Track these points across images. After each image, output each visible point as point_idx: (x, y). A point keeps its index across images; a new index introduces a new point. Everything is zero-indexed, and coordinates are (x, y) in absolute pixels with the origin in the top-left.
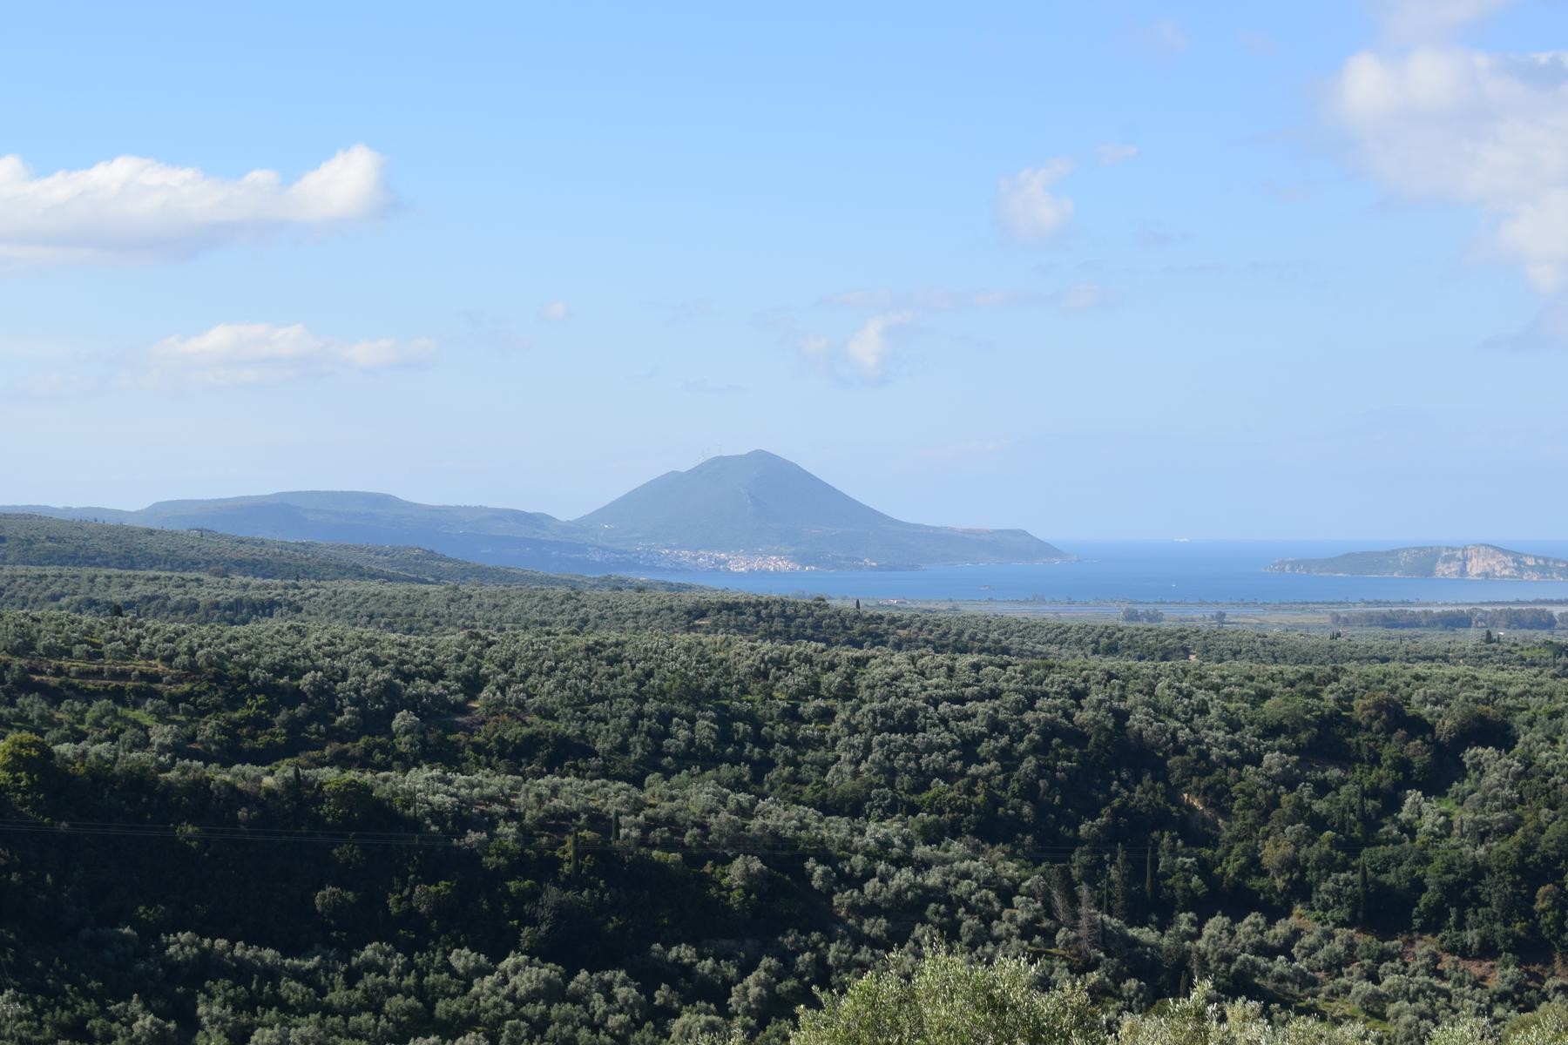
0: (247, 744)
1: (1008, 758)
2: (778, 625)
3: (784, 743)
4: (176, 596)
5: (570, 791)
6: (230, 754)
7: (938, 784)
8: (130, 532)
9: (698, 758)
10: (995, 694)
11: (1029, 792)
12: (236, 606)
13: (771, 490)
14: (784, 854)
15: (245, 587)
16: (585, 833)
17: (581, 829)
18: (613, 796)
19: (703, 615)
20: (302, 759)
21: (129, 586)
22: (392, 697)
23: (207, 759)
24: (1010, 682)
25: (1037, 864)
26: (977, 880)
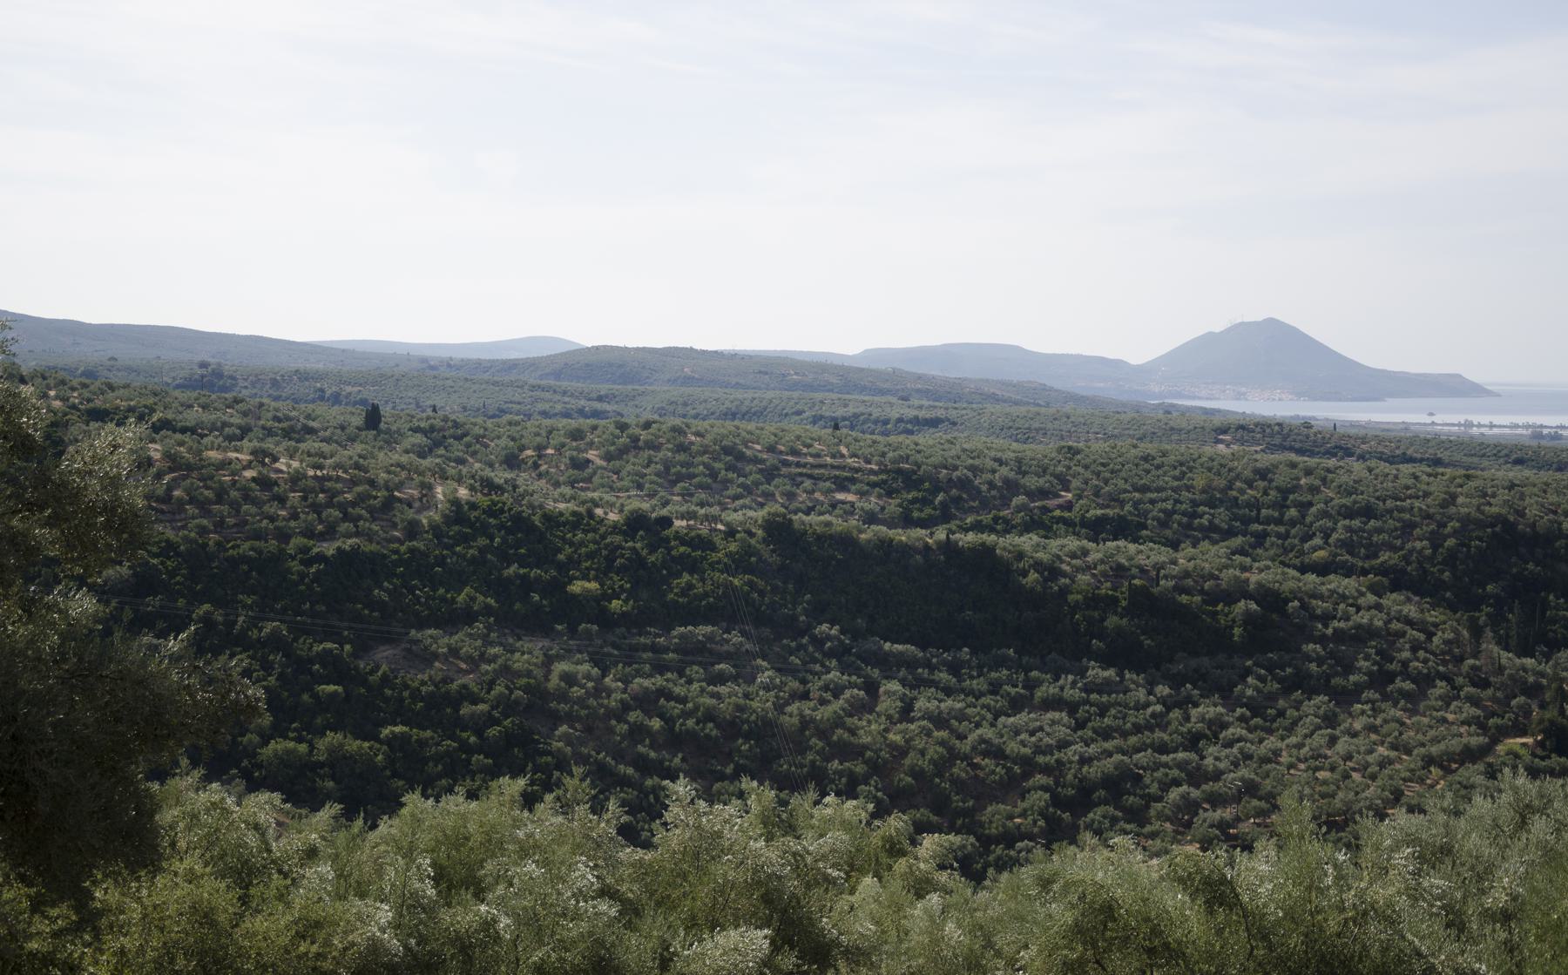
0: (916, 514)
1: (1436, 540)
2: (1277, 440)
3: (424, 910)
4: (559, 407)
5: (1126, 550)
6: (907, 521)
7: (1384, 556)
8: (850, 369)
9: (1214, 533)
10: (1426, 494)
11: (1451, 559)
12: (916, 421)
13: (1275, 346)
14: (1271, 600)
15: (921, 407)
16: (1136, 582)
17: (1134, 577)
18: (1160, 554)
19: (1225, 432)
20: (953, 525)
21: (846, 406)
22: (1011, 487)
23: (891, 525)
24: (1437, 488)
25: (1455, 612)
26: (1271, 948)
